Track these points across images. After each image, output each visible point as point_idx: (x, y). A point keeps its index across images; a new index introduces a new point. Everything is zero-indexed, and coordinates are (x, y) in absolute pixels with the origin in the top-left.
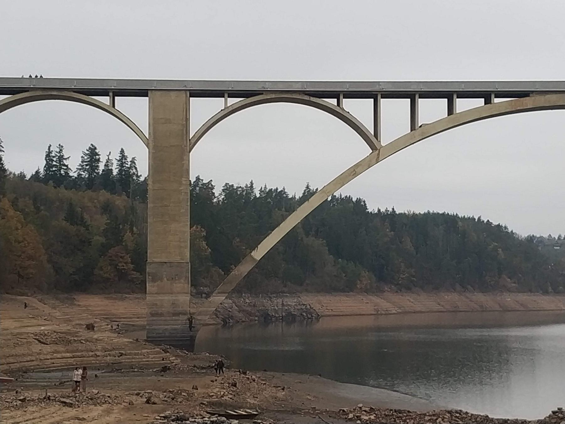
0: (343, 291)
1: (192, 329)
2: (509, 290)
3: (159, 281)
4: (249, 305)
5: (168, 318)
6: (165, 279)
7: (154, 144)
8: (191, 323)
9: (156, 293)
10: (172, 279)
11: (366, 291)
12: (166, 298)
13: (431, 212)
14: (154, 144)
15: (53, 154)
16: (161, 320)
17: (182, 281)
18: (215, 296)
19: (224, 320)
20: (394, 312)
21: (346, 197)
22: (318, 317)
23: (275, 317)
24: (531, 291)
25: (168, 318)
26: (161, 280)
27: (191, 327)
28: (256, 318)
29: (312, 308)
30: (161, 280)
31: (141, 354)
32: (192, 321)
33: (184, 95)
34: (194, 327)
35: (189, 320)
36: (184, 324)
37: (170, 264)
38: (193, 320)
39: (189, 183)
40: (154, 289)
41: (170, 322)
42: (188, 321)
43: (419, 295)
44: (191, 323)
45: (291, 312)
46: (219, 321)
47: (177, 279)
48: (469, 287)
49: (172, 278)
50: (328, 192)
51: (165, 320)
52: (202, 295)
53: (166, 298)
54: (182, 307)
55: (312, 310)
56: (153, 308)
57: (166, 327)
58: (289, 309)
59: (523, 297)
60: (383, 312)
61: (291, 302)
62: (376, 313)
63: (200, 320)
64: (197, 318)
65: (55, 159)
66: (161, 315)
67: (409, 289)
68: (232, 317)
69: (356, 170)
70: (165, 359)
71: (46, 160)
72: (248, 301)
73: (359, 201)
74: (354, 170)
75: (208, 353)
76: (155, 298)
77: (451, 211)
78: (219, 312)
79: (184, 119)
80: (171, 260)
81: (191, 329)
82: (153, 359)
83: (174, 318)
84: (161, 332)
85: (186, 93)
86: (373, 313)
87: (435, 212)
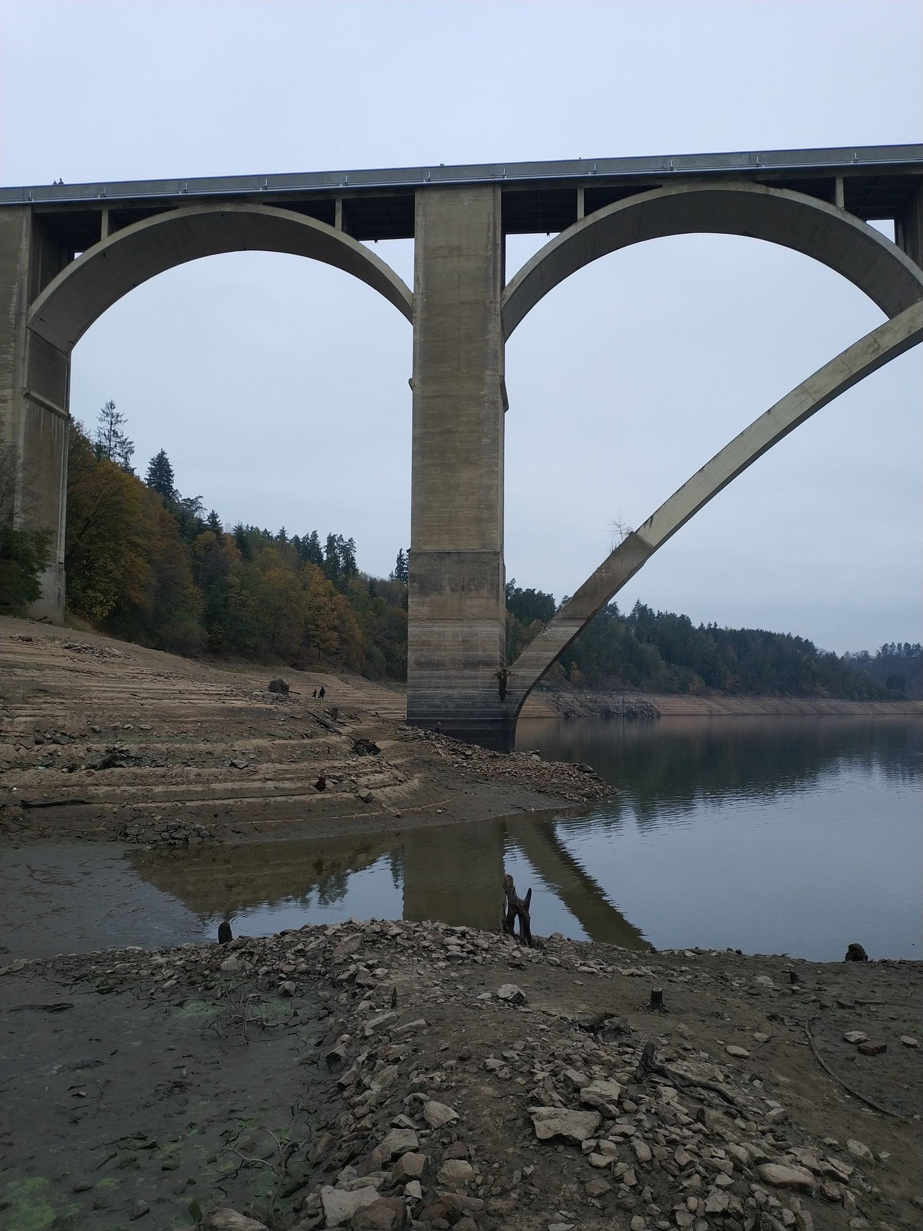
0: (677, 693)
1: (507, 697)
2: (823, 697)
3: (435, 593)
4: (591, 701)
5: (454, 673)
6: (448, 589)
7: (425, 300)
8: (503, 684)
9: (428, 619)
10: (463, 588)
11: (697, 694)
12: (449, 629)
13: (746, 629)
14: (425, 300)
15: (404, 557)
16: (441, 677)
17: (484, 593)
18: (556, 626)
19: (566, 714)
20: (726, 713)
21: (671, 614)
22: (659, 715)
23: (616, 713)
24: (840, 697)
25: (454, 673)
26: (439, 589)
27: (503, 693)
28: (598, 714)
29: (653, 706)
30: (439, 589)
31: (219, 761)
32: (505, 678)
33: (490, 197)
34: (509, 693)
35: (499, 678)
36: (488, 685)
37: (459, 556)
38: (508, 678)
39: (499, 382)
40: (425, 611)
41: (458, 681)
42: (496, 680)
43: (744, 700)
44: (503, 684)
45: (632, 709)
46: (561, 714)
47: (473, 587)
48: (787, 693)
49: (463, 587)
50: (815, 392)
51: (448, 677)
52: (542, 688)
53: (450, 629)
54: (484, 650)
55: (652, 708)
56: (421, 650)
57: (450, 692)
58: (630, 706)
59: (835, 703)
60: (716, 713)
61: (632, 699)
62: (709, 714)
63: (524, 678)
64: (516, 673)
65: (406, 562)
66: (439, 665)
67: (734, 693)
68: (574, 712)
69: (879, 341)
70: (329, 783)
71: (398, 563)
72: (588, 697)
73: (683, 616)
74: (875, 341)
75: (537, 753)
76: (426, 629)
77: (766, 628)
78: (561, 705)
79: (490, 246)
80: (462, 548)
81: (502, 698)
82: (270, 784)
83: (466, 671)
84: (437, 702)
85: (494, 192)
86: (707, 713)
87: (749, 629)
